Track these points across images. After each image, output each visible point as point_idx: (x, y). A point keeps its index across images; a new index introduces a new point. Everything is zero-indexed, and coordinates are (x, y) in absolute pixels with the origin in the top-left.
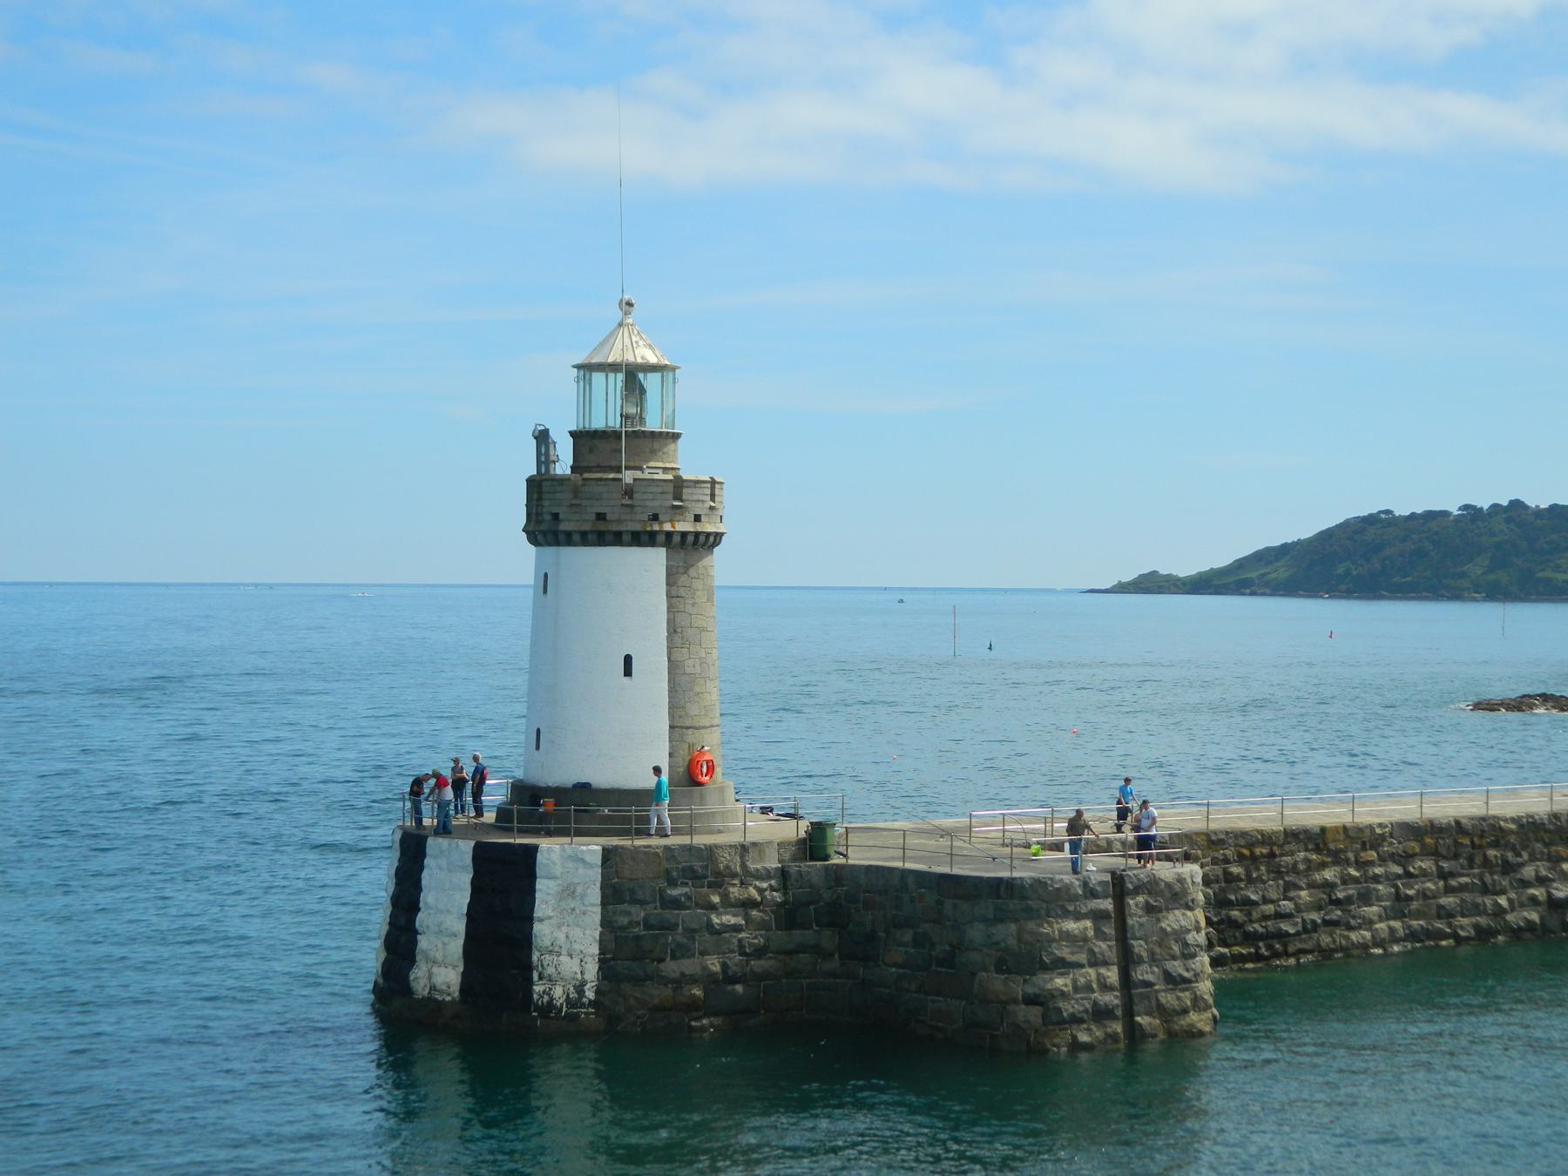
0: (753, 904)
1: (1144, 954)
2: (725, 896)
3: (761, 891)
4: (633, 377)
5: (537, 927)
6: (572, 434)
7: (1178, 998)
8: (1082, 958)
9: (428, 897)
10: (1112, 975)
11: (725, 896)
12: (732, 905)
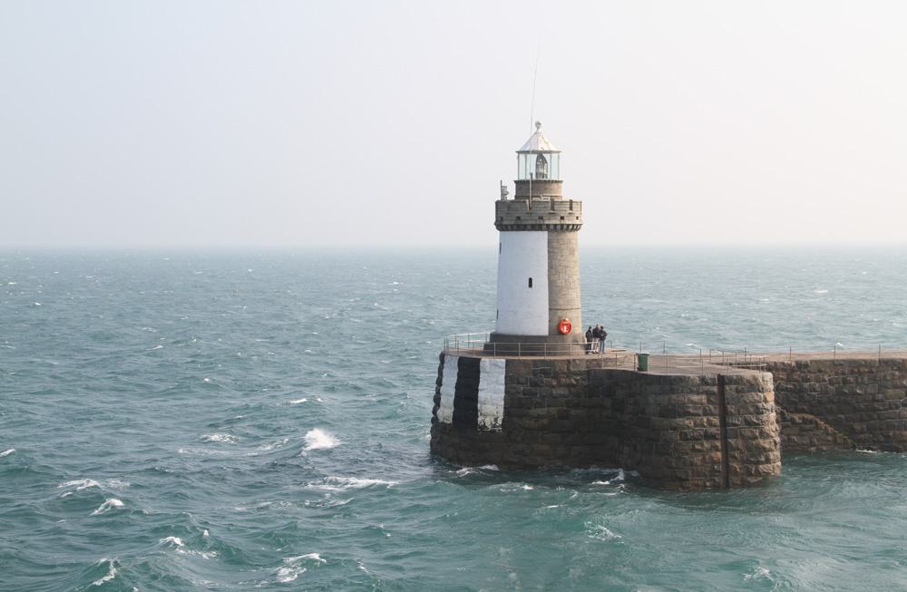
0: (573, 386)
2: (559, 382)
4: (541, 157)
5: (480, 394)
6: (515, 182)
7: (752, 432)
10: (716, 421)
11: (559, 382)
12: (562, 386)
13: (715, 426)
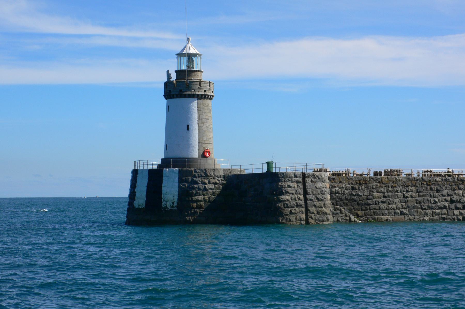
1: (311, 193)
3: (218, 180)
4: (190, 56)
5: (163, 189)
6: (176, 71)
8: (294, 192)
9: (138, 184)
10: (302, 197)
13: (301, 200)
